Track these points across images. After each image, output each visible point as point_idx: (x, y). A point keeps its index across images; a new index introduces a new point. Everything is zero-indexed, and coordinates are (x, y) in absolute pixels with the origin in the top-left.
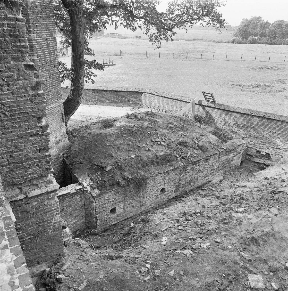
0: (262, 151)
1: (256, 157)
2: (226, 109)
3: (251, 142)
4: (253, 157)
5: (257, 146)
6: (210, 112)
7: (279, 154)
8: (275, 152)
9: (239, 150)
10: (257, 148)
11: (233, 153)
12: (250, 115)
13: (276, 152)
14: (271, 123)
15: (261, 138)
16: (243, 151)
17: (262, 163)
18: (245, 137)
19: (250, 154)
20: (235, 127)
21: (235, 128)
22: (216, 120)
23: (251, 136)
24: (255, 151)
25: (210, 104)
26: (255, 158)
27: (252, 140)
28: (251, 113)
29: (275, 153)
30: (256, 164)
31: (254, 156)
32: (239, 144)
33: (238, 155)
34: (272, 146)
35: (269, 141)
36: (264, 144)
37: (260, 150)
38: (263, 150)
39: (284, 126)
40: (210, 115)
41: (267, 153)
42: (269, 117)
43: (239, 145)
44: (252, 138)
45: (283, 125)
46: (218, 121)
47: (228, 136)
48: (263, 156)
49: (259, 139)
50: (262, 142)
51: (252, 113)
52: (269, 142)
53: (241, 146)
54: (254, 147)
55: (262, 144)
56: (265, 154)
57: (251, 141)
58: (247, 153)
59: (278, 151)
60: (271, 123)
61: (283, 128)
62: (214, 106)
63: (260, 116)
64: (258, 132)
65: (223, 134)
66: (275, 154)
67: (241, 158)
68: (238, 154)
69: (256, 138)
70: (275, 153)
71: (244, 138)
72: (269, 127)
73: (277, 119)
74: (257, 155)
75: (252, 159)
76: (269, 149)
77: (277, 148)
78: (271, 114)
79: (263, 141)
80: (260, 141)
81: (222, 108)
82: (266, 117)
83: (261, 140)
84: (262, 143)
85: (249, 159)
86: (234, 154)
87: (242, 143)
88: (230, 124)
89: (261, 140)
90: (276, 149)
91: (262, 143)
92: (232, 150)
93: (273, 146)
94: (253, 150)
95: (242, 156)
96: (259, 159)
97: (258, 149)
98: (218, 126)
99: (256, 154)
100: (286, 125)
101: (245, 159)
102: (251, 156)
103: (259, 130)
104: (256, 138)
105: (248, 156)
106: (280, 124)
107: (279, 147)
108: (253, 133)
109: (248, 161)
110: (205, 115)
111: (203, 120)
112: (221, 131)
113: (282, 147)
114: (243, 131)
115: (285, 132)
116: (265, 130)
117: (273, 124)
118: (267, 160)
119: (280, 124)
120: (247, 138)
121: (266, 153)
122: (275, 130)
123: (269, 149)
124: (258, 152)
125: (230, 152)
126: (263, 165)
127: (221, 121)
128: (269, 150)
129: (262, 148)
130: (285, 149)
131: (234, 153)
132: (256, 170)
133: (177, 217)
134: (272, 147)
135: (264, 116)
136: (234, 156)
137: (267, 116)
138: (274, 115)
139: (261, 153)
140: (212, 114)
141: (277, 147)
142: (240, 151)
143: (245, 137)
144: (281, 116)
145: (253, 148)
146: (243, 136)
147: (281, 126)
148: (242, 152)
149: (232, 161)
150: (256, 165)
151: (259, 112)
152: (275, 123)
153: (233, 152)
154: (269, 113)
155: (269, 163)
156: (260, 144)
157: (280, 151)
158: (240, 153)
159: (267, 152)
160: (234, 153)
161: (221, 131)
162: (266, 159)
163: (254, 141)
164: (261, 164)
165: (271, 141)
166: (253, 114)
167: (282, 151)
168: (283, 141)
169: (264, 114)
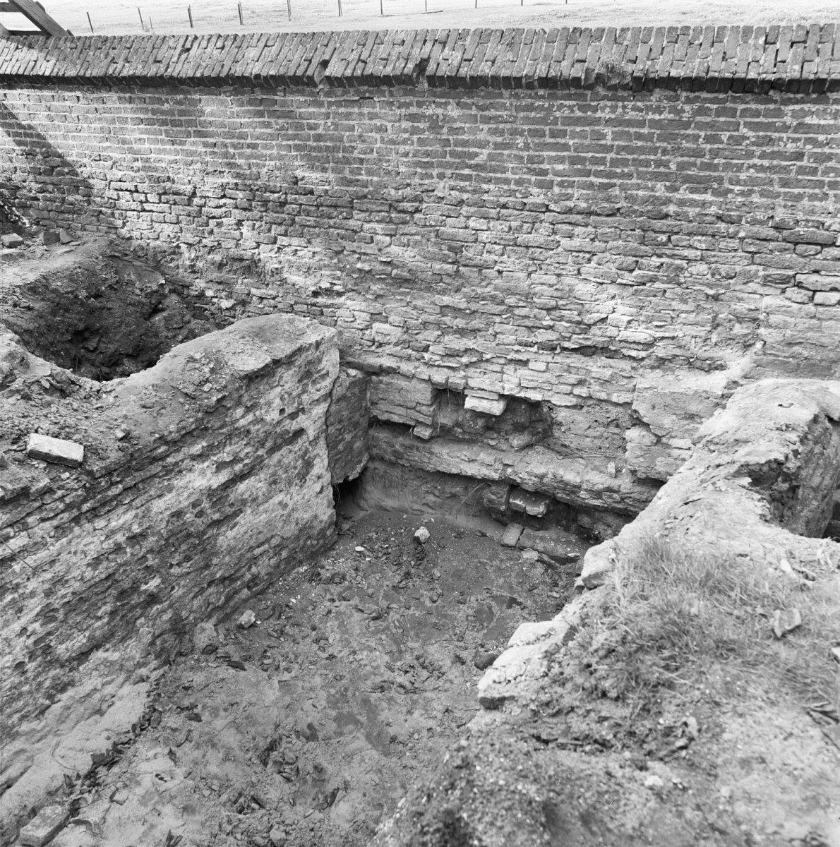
0: (472, 383)
1: (444, 434)
2: (126, 72)
3: (377, 326)
4: (418, 438)
5: (426, 349)
6: (40, 121)
7: (603, 396)
8: (573, 378)
9: (274, 416)
10: (428, 364)
11: (201, 457)
12: (310, 82)
13: (581, 383)
14: (496, 119)
15: (439, 276)
16: (320, 409)
17: (494, 482)
18: (328, 292)
19: (396, 419)
20: (232, 221)
21: (239, 223)
22: (97, 184)
23: (367, 275)
24: (423, 394)
25: (18, 54)
26: (437, 448)
27: (378, 307)
28: (315, 62)
29: (577, 391)
30: (458, 490)
31: (426, 433)
32: (252, 362)
33: (288, 455)
34: (542, 336)
35: (509, 292)
36: (476, 323)
37: (456, 379)
38: (478, 380)
39: (608, 131)
40: (49, 153)
41: (512, 402)
42: (465, 71)
43: (252, 378)
44: (376, 287)
45: (597, 121)
46: (114, 194)
47: (210, 302)
48: (491, 424)
49: (429, 289)
50: (457, 311)
51: (325, 64)
52: (511, 300)
53: (288, 377)
54: (409, 359)
55: (462, 332)
56: (497, 408)
57: (375, 317)
58: (375, 412)
59: (598, 367)
60: (496, 119)
61: (608, 149)
62: (46, 68)
63: (388, 70)
64: (407, 229)
65: (180, 289)
66: (574, 401)
67: (320, 466)
68: (272, 451)
69: (407, 281)
70: (577, 391)
71: (321, 300)
72: (476, 167)
73: (541, 71)
74: (446, 419)
75: (416, 456)
76: (525, 363)
77: (583, 350)
78: (483, 36)
79: (457, 300)
80: (444, 309)
81: (95, 72)
82: (444, 70)
83: (446, 300)
84: (460, 323)
85: (397, 454)
86: (220, 466)
87: (283, 349)
88: (196, 201)
89: (446, 300)
90: (576, 360)
91: (460, 323)
92: (175, 444)
93: (551, 336)
94: (403, 383)
95: (331, 446)
96: (466, 452)
97: (439, 377)
98: (124, 232)
99: (434, 416)
100: (632, 115)
101: (372, 458)
102: (404, 428)
103: (407, 206)
104: (407, 281)
105: (382, 435)
106: (578, 121)
107: (596, 336)
108: (372, 249)
109: (396, 473)
110: (21, 163)
111: (23, 207)
112: (158, 267)
113: (624, 334)
114: (295, 241)
115: (623, 188)
116: (461, 202)
117: (515, 132)
118: (529, 446)
119: (578, 121)
120: (340, 294)
121: (502, 396)
122: (540, 185)
123: (525, 363)
124: (447, 395)
125: (156, 468)
126: (503, 491)
127: (130, 186)
128: (523, 372)
129: (465, 360)
130: (649, 345)
131: (225, 456)
132: (459, 535)
133: (614, 185)
134: (543, 346)
135: (422, 65)
136: (223, 477)
137: (447, 61)
138: (511, 38)
139: (469, 403)
140: (57, 139)
141: (577, 341)
142: (293, 416)
143: (328, 292)
144: (573, 36)
145: (406, 367)
146: (309, 284)
147: (582, 135)
148: (311, 422)
149: (217, 523)
150: (454, 496)
151: (378, 38)
152: (527, 120)
153: (196, 449)
154: (462, 36)
155: (542, 477)
156: (446, 330)
157: (607, 373)
158: (300, 432)
159: (510, 388)
160: (225, 456)
161: (158, 267)
162: (517, 441)
163: (396, 308)
164: (487, 482)
165: (528, 296)
166: (334, 69)
167: (626, 365)
168: (628, 278)
169: (418, 54)
